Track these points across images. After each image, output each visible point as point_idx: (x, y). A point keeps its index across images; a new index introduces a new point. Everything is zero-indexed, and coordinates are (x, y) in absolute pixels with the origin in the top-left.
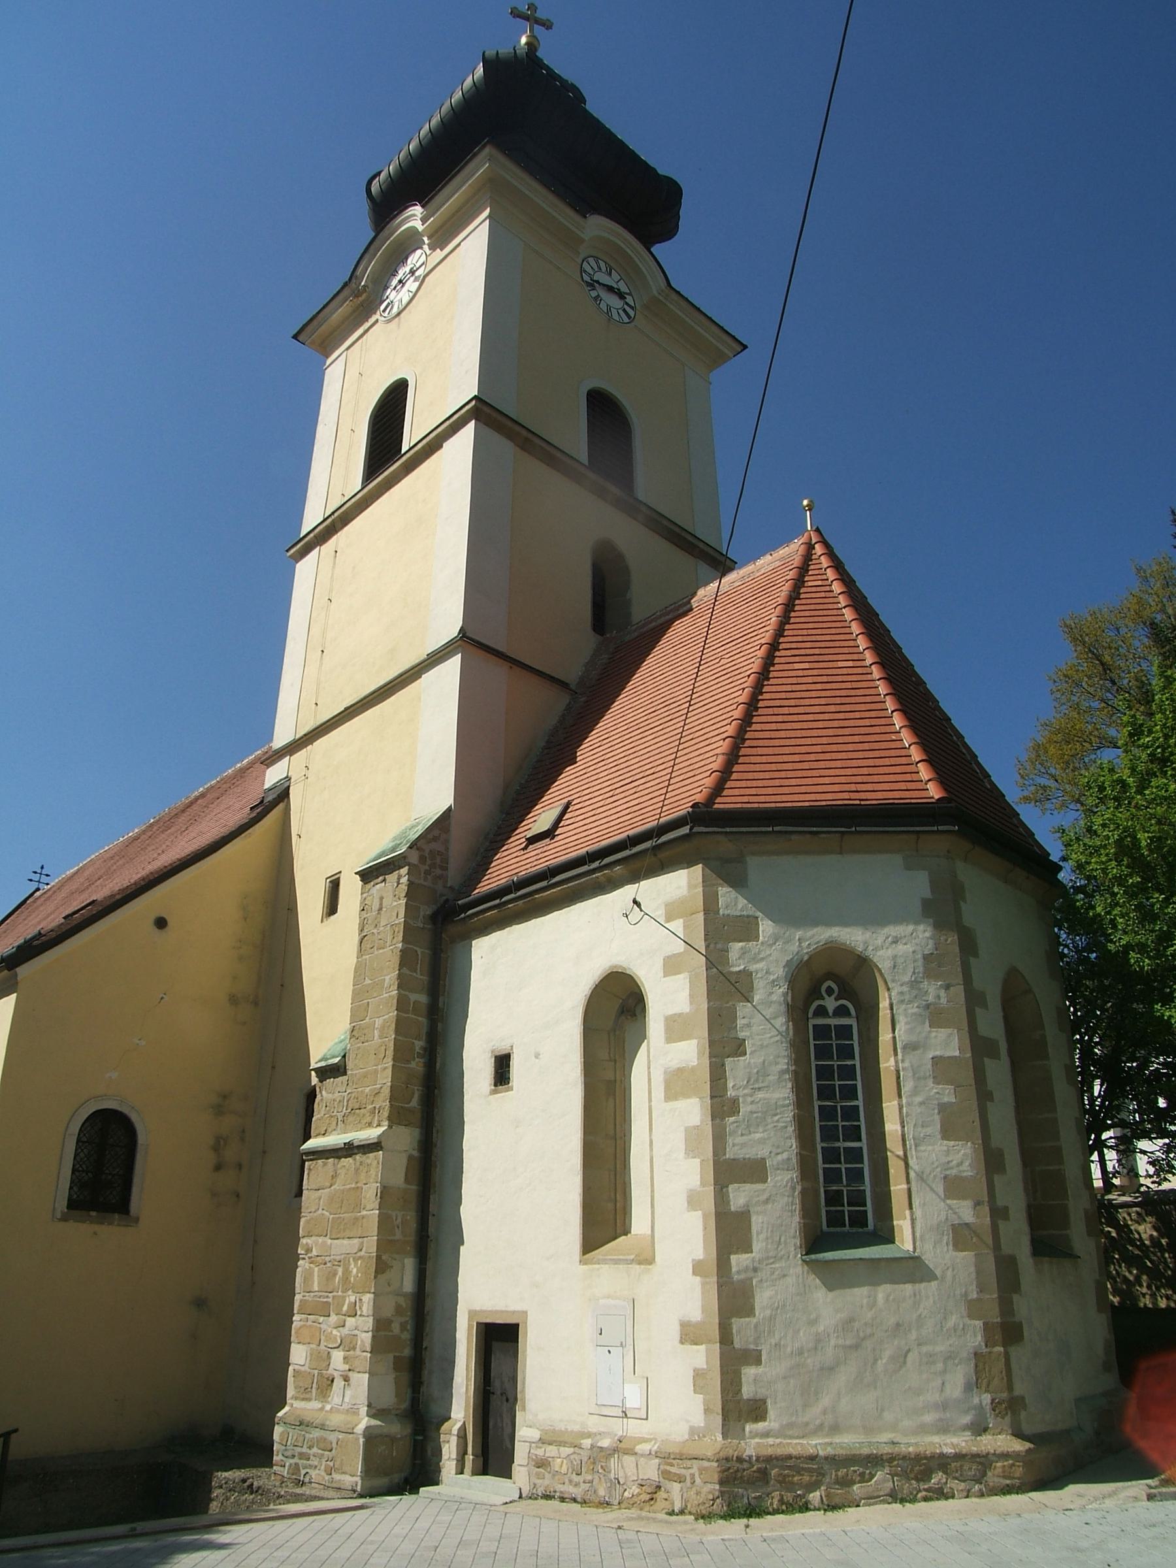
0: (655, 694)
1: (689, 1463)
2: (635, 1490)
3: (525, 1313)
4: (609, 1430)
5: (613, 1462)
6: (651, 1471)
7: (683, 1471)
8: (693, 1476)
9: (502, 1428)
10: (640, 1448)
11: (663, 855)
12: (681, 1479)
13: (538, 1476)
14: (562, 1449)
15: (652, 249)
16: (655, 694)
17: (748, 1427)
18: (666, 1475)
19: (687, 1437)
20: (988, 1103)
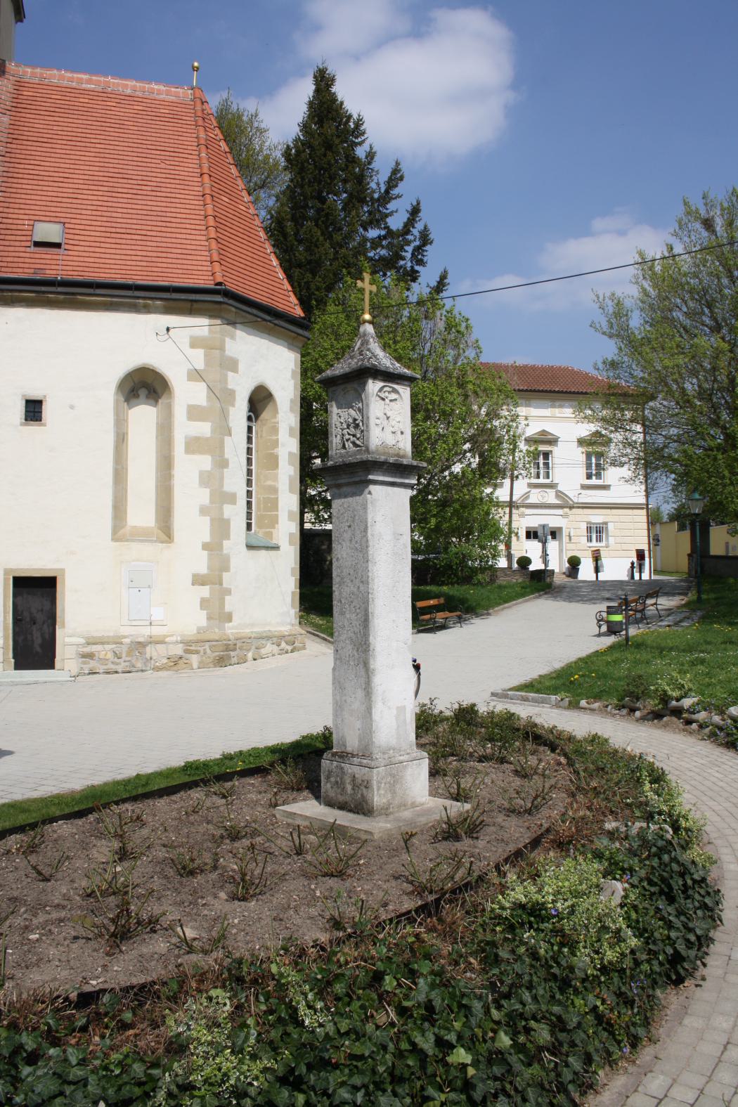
0: (244, 257)
1: (203, 644)
2: (165, 661)
3: (63, 570)
4: (144, 632)
5: (148, 649)
6: (178, 650)
7: (199, 648)
8: (204, 650)
9: (33, 641)
10: (167, 640)
11: (196, 306)
12: (197, 652)
13: (84, 663)
14: (105, 646)
15: (508, 500)
16: (244, 257)
17: (226, 625)
18: (187, 651)
19: (195, 632)
20: (230, 374)
